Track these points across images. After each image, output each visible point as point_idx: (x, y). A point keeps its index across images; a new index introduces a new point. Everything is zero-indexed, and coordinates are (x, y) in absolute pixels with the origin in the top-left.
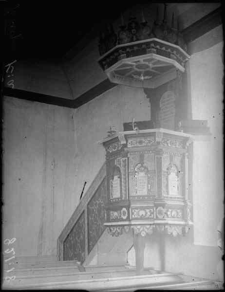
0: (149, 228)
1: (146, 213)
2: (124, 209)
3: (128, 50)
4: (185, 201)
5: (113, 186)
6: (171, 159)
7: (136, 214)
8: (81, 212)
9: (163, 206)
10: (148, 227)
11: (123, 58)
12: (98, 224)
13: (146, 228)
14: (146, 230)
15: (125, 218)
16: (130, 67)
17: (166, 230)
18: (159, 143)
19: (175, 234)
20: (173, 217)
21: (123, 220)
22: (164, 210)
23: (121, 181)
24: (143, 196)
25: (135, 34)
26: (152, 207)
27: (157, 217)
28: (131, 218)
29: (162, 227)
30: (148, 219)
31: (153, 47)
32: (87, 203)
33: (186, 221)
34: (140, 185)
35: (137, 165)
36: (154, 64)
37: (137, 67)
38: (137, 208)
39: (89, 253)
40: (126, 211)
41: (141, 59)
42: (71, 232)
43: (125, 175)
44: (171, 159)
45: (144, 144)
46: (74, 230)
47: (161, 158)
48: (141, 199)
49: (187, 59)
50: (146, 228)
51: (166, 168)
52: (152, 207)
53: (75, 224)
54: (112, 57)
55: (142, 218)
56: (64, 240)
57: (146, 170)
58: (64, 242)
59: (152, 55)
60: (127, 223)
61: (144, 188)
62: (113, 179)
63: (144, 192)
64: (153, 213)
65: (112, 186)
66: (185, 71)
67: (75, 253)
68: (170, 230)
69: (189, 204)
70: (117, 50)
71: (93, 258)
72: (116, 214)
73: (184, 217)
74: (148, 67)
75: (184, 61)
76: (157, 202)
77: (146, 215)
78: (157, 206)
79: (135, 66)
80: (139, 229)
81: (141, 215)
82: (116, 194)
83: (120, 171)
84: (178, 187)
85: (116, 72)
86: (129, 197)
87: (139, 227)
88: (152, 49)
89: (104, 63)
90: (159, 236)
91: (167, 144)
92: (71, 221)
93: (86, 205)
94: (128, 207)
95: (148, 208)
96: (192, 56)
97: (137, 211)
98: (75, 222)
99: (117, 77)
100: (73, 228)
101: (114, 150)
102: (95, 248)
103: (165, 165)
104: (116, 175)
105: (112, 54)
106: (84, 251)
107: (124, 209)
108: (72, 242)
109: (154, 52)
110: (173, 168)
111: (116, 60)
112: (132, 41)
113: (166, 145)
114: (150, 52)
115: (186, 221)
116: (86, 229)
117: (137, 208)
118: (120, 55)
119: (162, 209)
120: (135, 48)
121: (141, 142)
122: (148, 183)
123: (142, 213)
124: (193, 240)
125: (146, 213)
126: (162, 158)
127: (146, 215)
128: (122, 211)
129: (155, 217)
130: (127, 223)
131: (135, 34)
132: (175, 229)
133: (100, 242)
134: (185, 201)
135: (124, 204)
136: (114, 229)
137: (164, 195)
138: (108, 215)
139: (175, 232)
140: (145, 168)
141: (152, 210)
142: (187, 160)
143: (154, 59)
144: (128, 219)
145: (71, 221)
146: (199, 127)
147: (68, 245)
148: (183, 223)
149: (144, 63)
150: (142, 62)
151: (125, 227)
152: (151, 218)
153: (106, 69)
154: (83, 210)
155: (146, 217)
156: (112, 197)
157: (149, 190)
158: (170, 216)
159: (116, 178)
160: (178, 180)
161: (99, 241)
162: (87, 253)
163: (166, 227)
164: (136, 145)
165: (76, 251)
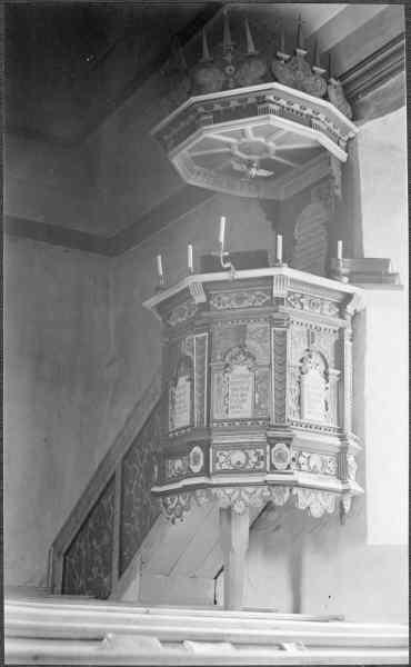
0: (255, 492)
1: (248, 458)
2: (197, 449)
3: (217, 107)
4: (343, 438)
5: (177, 400)
6: (311, 338)
7: (224, 460)
8: (110, 476)
9: (288, 441)
10: (250, 490)
11: (207, 123)
12: (145, 502)
13: (247, 493)
14: (246, 497)
15: (196, 469)
16: (227, 150)
17: (294, 499)
18: (280, 301)
19: (316, 512)
20: (312, 472)
21: (191, 475)
22: (292, 453)
23: (192, 387)
24: (243, 420)
25: (232, 76)
26: (262, 445)
27: (273, 467)
28: (211, 470)
29: (285, 492)
30: (252, 472)
31: (273, 103)
32: (121, 455)
33: (344, 482)
34: (237, 395)
35: (230, 350)
36: (278, 143)
37: (241, 148)
38: (226, 447)
39: (121, 573)
40: (202, 455)
41: (249, 125)
42: (82, 529)
43: (201, 372)
44: (311, 338)
45: (246, 303)
46: (91, 525)
47: (285, 333)
48: (240, 425)
49: (351, 135)
50: (247, 493)
51: (300, 357)
52: (262, 445)
53: (94, 508)
54: (182, 124)
55: (237, 470)
56: (64, 551)
57: (249, 361)
58: (66, 554)
59: (269, 118)
60: (202, 480)
61: (244, 401)
62: (176, 385)
63: (245, 410)
64: (262, 458)
65: (173, 402)
66: (348, 158)
67: (90, 579)
68: (303, 500)
69: (351, 443)
70: (192, 109)
71: (129, 583)
72: (178, 463)
73: (341, 474)
74: (266, 150)
75: (346, 138)
76: (273, 429)
77: (247, 462)
78: (272, 441)
79: (236, 147)
80: (230, 496)
81: (234, 462)
82: (181, 418)
83: (191, 366)
84: (326, 404)
85: (196, 160)
86: (208, 422)
87: (229, 491)
88: (271, 105)
89: (166, 137)
90: (279, 527)
91: (302, 305)
92: (84, 502)
93: (118, 461)
94: (206, 446)
95: (253, 446)
96: (363, 127)
97: (226, 453)
98: (93, 502)
99: (205, 174)
100: (86, 521)
101: (180, 320)
102: (136, 561)
103: (294, 353)
104: (184, 374)
105: (181, 117)
106: (108, 572)
107: (197, 449)
108: (84, 553)
109: (274, 112)
110: (316, 359)
111: (193, 128)
112: (225, 88)
113: (298, 306)
114: (266, 111)
115: (344, 482)
116: (117, 517)
117: (226, 447)
118: (199, 116)
119: (286, 449)
120: (234, 104)
121: (240, 300)
122: (256, 390)
123: (238, 457)
124: (364, 536)
125: (248, 458)
126: (289, 335)
127: (247, 462)
128: (191, 454)
129: (268, 469)
130: (202, 480)
131: (232, 76)
132: (317, 500)
133: (145, 547)
134: (343, 438)
135: (202, 435)
136: (172, 501)
137: (291, 416)
138: (163, 469)
139: (318, 506)
140: (249, 355)
141: (262, 451)
142: (348, 343)
143: (280, 129)
144: (205, 472)
145: (84, 502)
146: (374, 273)
147: (73, 561)
148: (339, 486)
149: (274, 157)
150: (251, 137)
151: (198, 492)
152: (260, 471)
153: (172, 148)
154: (112, 472)
155: (248, 467)
156: (173, 427)
157: (256, 407)
158: (303, 467)
159: (182, 381)
160: (327, 388)
161: (145, 543)
162: (115, 572)
163: (295, 491)
164: (227, 306)
165: (90, 573)
